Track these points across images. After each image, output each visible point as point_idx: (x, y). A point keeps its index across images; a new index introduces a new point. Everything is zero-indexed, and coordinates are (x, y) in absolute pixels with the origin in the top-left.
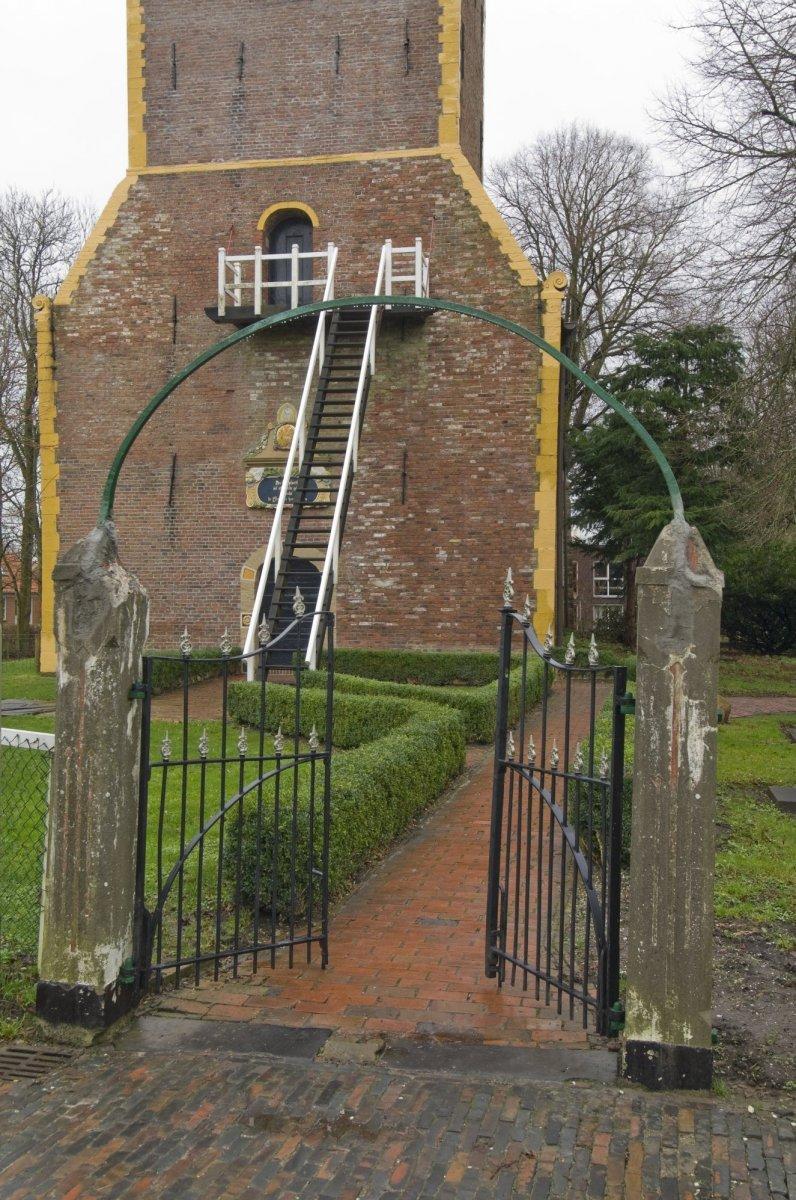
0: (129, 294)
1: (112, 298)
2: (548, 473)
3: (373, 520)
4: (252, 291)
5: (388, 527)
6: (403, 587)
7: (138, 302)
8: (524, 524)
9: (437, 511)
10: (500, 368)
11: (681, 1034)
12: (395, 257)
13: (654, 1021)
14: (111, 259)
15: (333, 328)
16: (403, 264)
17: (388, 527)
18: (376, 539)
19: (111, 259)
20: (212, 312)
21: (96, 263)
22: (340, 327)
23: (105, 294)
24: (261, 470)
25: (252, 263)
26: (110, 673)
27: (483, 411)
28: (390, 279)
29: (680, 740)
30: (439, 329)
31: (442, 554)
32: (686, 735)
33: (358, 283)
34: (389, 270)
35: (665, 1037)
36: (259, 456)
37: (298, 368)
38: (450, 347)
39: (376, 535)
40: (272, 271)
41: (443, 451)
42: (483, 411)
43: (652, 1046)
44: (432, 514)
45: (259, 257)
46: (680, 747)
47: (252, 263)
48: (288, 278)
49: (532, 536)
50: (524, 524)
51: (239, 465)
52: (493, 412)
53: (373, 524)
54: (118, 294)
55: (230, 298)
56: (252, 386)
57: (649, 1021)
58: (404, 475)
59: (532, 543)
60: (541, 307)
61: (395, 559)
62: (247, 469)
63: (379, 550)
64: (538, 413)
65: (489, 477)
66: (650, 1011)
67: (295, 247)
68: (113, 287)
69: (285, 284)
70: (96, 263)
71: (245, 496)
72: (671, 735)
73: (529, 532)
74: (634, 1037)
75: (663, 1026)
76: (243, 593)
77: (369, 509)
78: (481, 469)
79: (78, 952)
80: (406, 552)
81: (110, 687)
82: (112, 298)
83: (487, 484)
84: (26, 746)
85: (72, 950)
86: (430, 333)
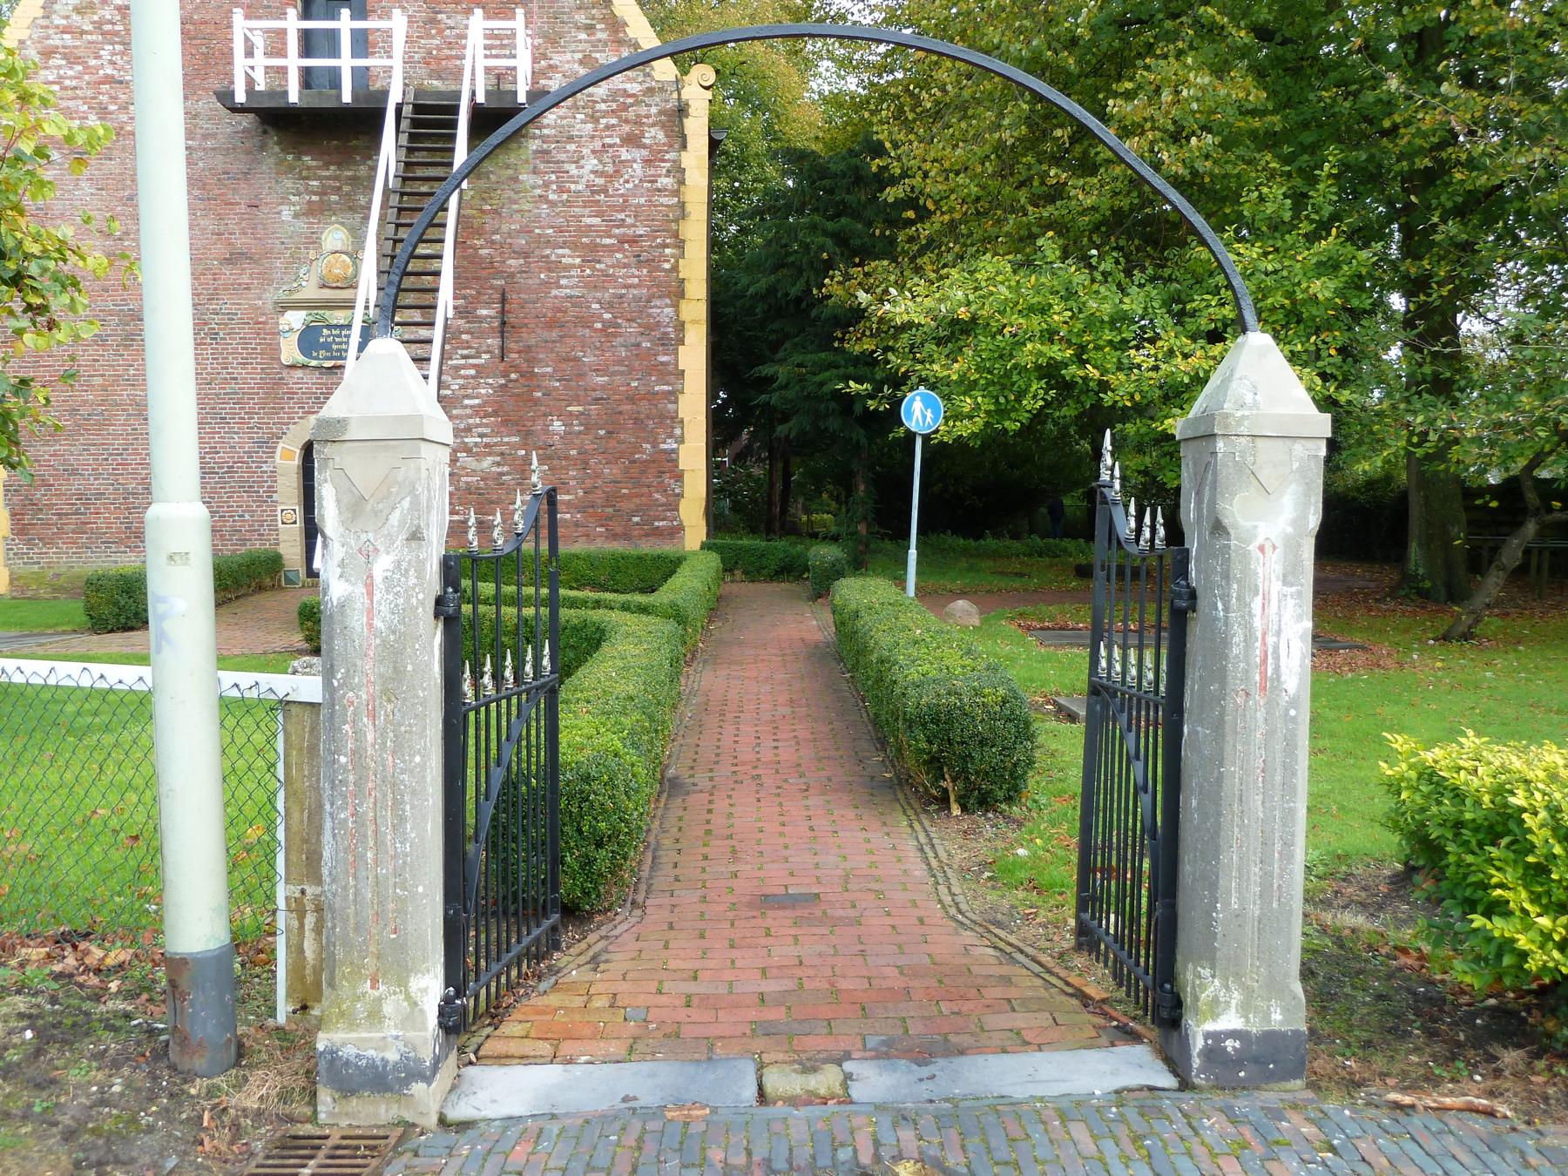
0: (97, 68)
1: (70, 73)
2: (695, 322)
3: (461, 381)
4: (283, 71)
5: (483, 391)
6: (506, 469)
7: (109, 80)
8: (666, 388)
9: (549, 369)
10: (630, 186)
11: (1267, 1017)
12: (491, 34)
13: (1234, 1003)
14: (67, 17)
15: (405, 124)
16: (500, 43)
17: (483, 391)
18: (466, 407)
19: (67, 17)
20: (225, 97)
21: (45, 22)
22: (415, 123)
23: (59, 67)
24: (302, 314)
25: (282, 33)
26: (414, 581)
27: (608, 241)
28: (482, 63)
29: (1271, 640)
30: (546, 131)
31: (558, 426)
32: (1278, 633)
33: (434, 66)
34: (481, 52)
35: (1247, 1021)
36: (297, 296)
37: (350, 178)
38: (563, 157)
39: (467, 402)
40: (308, 44)
41: (555, 292)
42: (608, 241)
43: (1234, 1034)
44: (543, 375)
45: (293, 23)
46: (1270, 650)
47: (282, 33)
48: (335, 52)
49: (676, 402)
50: (666, 388)
51: (270, 306)
52: (621, 242)
53: (462, 387)
54: (80, 68)
55: (250, 82)
56: (284, 200)
57: (1228, 1003)
58: (504, 323)
59: (677, 412)
60: (682, 111)
61: (495, 433)
62: (282, 313)
63: (471, 421)
64: (680, 245)
65: (619, 326)
66: (1227, 988)
67: (345, 13)
68: (72, 58)
69: (386, 62)
70: (45, 22)
71: (278, 350)
72: (1259, 635)
73: (673, 396)
74: (1210, 1026)
75: (1245, 1009)
76: (280, 480)
77: (457, 368)
78: (607, 316)
79: (382, 988)
80: (505, 423)
81: (414, 601)
82: (70, 73)
83: (615, 335)
84: (235, 693)
85: (373, 987)
86: (534, 137)
